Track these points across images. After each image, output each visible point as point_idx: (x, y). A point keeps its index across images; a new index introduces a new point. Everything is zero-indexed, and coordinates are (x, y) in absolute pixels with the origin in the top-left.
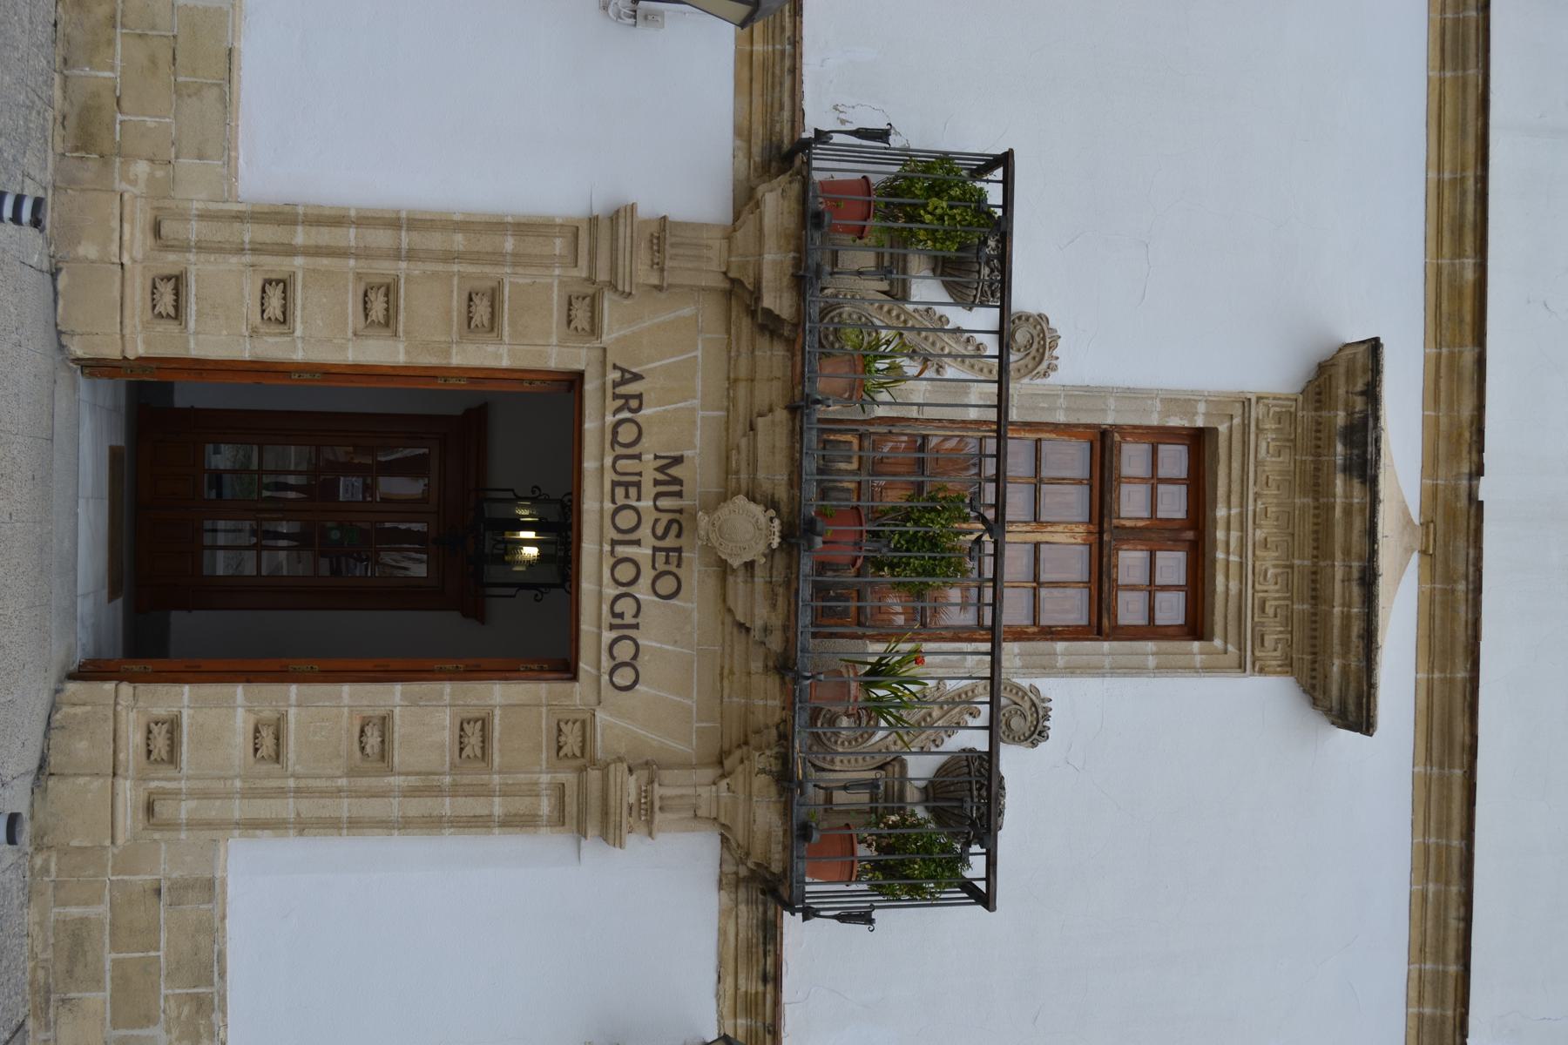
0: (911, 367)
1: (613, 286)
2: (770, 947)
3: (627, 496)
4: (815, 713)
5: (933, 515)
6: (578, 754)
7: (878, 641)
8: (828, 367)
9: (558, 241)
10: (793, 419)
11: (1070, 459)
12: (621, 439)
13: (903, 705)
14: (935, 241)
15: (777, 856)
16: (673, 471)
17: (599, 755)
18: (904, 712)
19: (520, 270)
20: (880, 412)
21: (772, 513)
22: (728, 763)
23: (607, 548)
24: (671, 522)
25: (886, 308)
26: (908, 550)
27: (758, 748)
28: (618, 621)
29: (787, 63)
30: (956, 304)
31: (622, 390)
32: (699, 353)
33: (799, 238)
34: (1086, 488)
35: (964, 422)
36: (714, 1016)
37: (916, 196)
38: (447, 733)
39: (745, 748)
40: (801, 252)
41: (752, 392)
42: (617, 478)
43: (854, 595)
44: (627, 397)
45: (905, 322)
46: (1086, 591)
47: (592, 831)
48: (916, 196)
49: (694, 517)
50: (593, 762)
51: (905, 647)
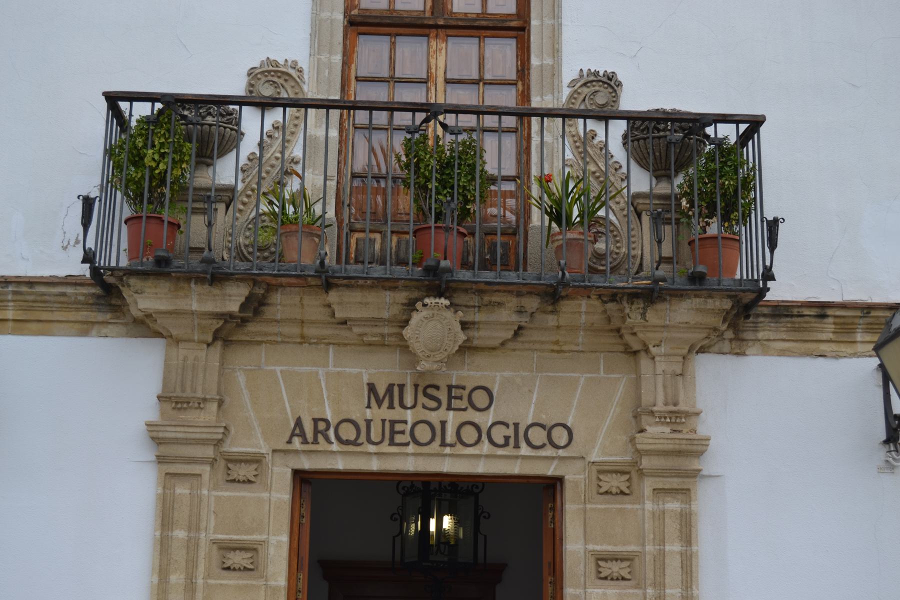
0: (294, 185)
1: (218, 443)
2: (795, 311)
3: (403, 432)
4: (593, 270)
5: (422, 165)
6: (627, 477)
7: (529, 217)
8: (291, 255)
9: (178, 491)
10: (337, 286)
11: (373, 53)
12: (352, 437)
13: (585, 192)
14: (182, 161)
15: (718, 303)
16: (381, 391)
17: (628, 458)
18: (592, 195)
19: (203, 525)
20: (331, 213)
21: (419, 305)
22: (636, 346)
23: (448, 450)
24: (426, 394)
25: (241, 207)
26: (452, 188)
27: (623, 319)
28: (512, 441)
29: (24, 289)
30: (237, 147)
31: (310, 435)
32: (278, 369)
33: (178, 279)
34: (399, 39)
35: (340, 142)
36: (855, 360)
37: (143, 177)
38: (610, 592)
39: (623, 331)
40: (191, 277)
41: (313, 322)
42: (387, 441)
43: (489, 238)
44: (316, 432)
45: (253, 190)
46: (487, 40)
47: (695, 464)
48: (143, 177)
49: (422, 374)
50: (635, 463)
51: (535, 191)
